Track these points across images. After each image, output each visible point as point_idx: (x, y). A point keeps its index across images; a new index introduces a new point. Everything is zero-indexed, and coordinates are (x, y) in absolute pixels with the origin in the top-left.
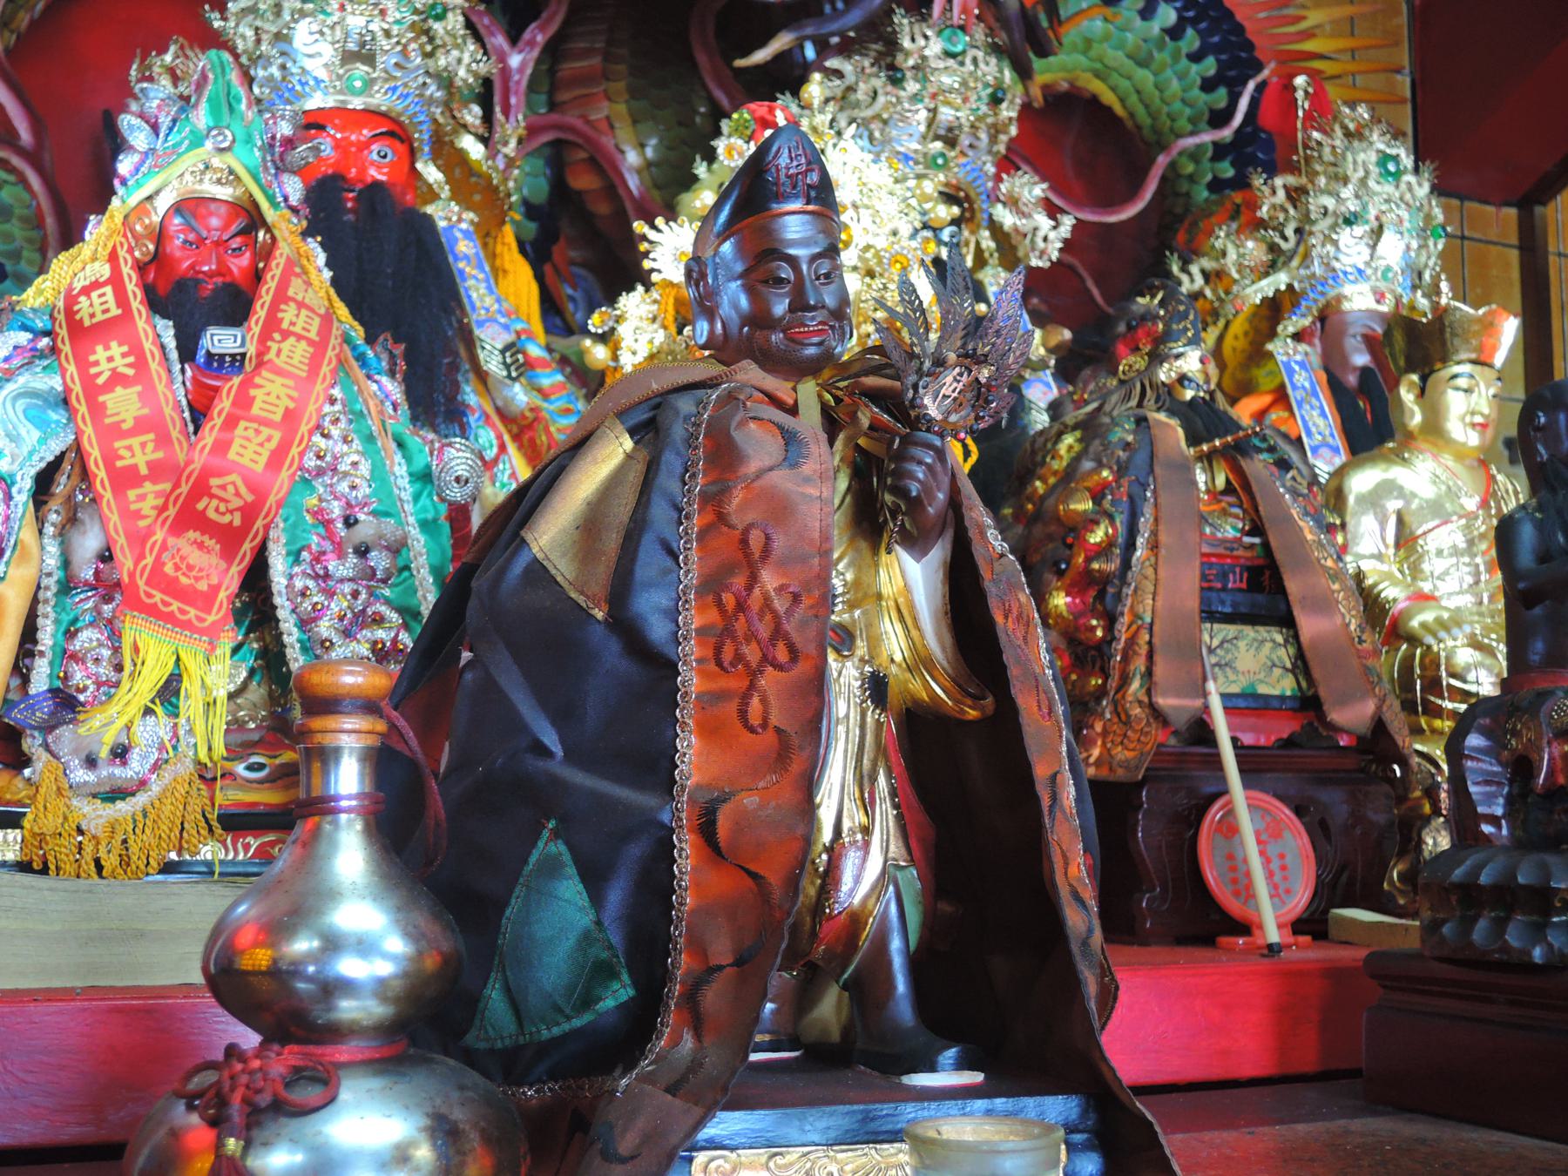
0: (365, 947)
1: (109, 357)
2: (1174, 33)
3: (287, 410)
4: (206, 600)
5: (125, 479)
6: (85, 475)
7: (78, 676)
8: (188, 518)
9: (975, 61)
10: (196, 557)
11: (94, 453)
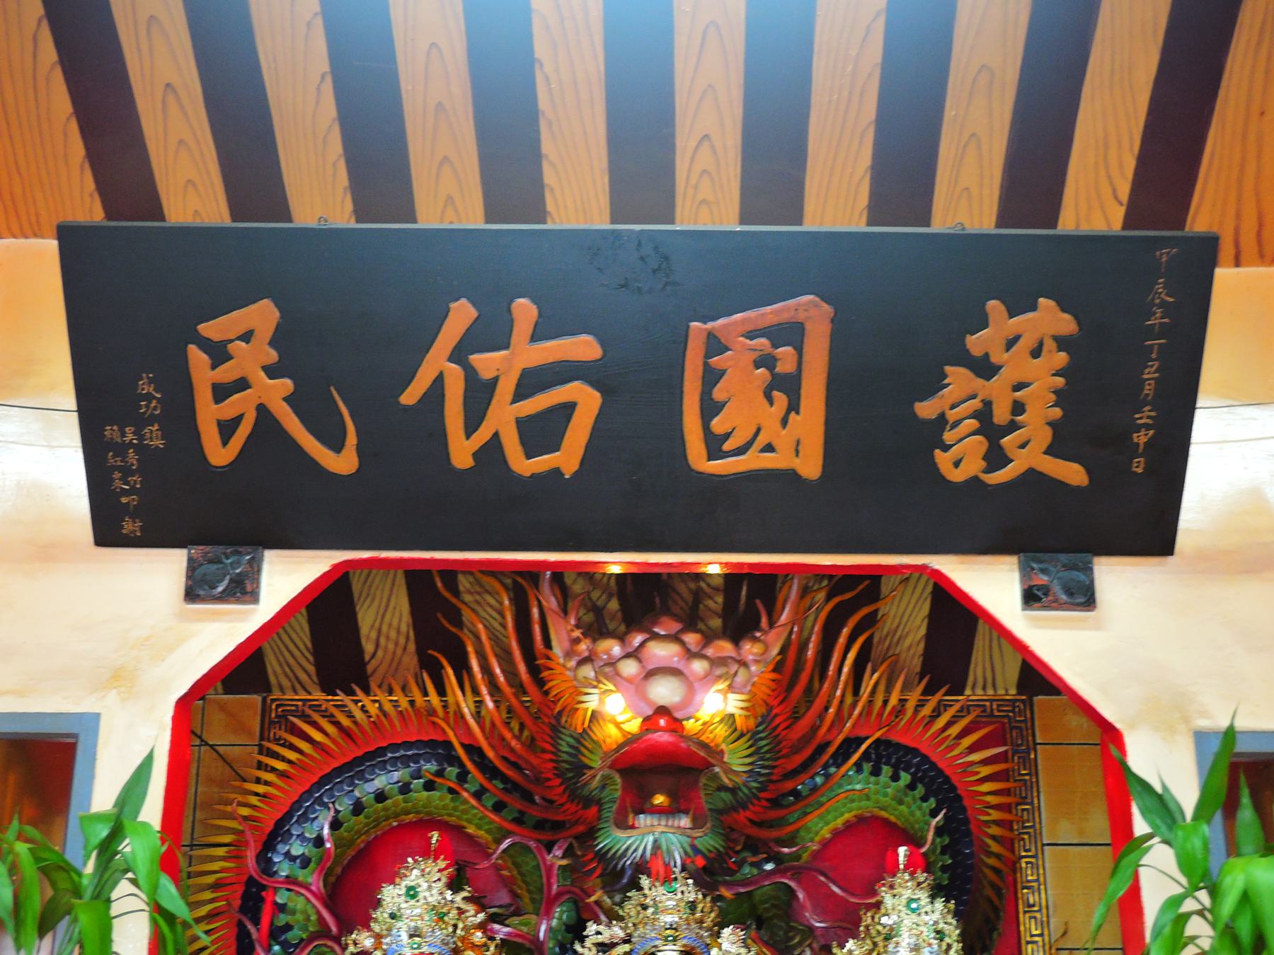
2: (911, 786)
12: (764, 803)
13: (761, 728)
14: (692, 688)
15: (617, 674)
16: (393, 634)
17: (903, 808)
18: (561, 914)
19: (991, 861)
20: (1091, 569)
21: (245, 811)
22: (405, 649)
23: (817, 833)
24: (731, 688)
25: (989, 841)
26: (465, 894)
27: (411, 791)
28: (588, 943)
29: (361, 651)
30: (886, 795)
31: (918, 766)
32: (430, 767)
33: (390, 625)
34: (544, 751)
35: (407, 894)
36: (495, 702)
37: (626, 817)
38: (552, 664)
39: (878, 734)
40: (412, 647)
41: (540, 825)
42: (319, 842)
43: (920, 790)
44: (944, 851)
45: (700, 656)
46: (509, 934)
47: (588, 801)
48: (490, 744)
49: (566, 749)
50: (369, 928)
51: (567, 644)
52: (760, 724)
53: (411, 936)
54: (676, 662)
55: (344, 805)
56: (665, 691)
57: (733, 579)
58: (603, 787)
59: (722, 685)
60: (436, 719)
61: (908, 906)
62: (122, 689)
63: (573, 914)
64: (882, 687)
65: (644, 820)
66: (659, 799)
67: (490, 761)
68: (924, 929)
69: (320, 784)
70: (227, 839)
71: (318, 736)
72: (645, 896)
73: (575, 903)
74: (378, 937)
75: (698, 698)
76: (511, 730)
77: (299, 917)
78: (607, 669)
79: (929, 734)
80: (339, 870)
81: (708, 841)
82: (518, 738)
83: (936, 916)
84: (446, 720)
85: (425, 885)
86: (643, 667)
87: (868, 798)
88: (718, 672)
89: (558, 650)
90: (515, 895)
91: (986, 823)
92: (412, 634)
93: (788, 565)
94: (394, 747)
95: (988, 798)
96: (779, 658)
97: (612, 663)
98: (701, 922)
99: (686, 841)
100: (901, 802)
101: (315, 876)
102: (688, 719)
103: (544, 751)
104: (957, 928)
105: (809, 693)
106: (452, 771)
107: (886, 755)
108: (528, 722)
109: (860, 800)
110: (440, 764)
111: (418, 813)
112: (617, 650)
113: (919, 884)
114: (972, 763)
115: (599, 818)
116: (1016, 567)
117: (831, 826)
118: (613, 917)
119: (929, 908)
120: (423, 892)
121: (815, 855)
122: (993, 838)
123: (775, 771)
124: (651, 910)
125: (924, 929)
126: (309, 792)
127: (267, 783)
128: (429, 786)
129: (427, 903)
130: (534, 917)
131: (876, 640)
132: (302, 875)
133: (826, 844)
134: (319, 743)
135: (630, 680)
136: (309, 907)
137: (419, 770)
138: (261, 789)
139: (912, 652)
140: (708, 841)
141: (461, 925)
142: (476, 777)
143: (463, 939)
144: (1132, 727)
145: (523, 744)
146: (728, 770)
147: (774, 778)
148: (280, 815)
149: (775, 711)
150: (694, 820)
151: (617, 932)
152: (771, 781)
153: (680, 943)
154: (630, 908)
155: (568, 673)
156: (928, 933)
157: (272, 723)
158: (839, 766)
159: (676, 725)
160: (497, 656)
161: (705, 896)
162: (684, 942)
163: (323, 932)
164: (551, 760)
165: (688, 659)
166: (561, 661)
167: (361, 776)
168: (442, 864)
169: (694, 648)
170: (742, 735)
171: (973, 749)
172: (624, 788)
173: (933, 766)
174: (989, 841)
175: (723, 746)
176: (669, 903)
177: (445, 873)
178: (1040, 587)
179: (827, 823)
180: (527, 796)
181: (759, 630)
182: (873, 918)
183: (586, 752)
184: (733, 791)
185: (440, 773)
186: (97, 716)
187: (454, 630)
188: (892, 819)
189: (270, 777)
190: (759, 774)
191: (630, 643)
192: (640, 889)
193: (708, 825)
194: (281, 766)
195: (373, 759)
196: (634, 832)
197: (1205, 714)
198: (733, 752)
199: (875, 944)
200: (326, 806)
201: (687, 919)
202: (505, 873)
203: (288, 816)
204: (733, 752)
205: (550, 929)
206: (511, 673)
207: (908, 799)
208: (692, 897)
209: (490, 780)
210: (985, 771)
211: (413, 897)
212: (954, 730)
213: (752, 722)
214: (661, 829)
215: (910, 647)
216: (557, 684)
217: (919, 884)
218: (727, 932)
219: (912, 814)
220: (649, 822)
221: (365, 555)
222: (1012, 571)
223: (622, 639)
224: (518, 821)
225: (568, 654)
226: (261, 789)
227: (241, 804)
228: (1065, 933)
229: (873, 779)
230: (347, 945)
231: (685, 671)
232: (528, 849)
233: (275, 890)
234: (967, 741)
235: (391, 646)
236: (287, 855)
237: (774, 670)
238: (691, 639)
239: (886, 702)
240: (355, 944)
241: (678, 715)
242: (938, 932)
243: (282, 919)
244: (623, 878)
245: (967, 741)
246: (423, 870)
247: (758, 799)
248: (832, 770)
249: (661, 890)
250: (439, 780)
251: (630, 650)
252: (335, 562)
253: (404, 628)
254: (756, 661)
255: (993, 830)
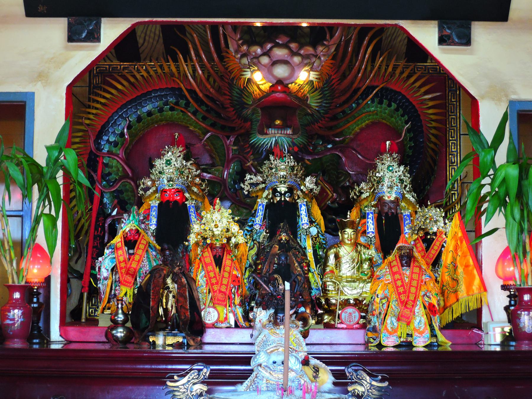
0: (121, 318)
1: (120, 252)
2: (397, 110)
3: (244, 182)
4: (130, 283)
5: (121, 268)
6: (117, 268)
7: (116, 292)
8: (127, 273)
9: (288, 162)
10: (129, 278)
11: (118, 265)
12: (326, 119)
13: (325, 86)
14: (293, 69)
15: (259, 62)
16: (152, 35)
17: (393, 119)
18: (233, 167)
19: (432, 145)
20: (470, 28)
21: (87, 122)
22: (158, 41)
23: (353, 130)
24: (312, 69)
25: (431, 136)
26: (192, 162)
27: (163, 111)
28: (246, 183)
29: (137, 42)
30: (385, 113)
31: (400, 100)
32: (172, 100)
33: (151, 31)
34: (225, 94)
35: (166, 163)
36: (202, 71)
37: (263, 129)
38: (229, 56)
39: (382, 86)
40: (161, 40)
41: (223, 128)
42: (122, 135)
43: (401, 111)
44: (410, 140)
45: (297, 54)
46: (210, 177)
47: (246, 119)
48: (201, 91)
49: (235, 94)
50: (149, 177)
51: (236, 46)
52: (325, 84)
53: (168, 181)
54: (287, 57)
55: (133, 118)
56: (281, 71)
57: (312, 27)
58: (253, 114)
59: (307, 68)
60: (175, 79)
61: (388, 168)
62: (43, 81)
63: (239, 166)
64: (384, 63)
65: (271, 131)
66: (278, 122)
67: (200, 97)
68: (395, 179)
69: (121, 108)
70: (80, 134)
71: (120, 87)
72: (272, 164)
73: (240, 162)
74: (153, 181)
75: (296, 74)
76: (210, 83)
77: (114, 169)
78: (255, 60)
79: (406, 85)
80: (131, 147)
81: (299, 140)
82: (213, 87)
83: (401, 173)
84: (179, 78)
85: (174, 159)
86: (271, 60)
87: (377, 114)
88: (306, 62)
89: (232, 49)
90: (212, 157)
91: (431, 128)
92: (161, 35)
93: (335, 24)
94: (156, 91)
95: (432, 117)
96: (334, 53)
97: (257, 57)
98: (296, 175)
99: (290, 140)
100: (392, 117)
101: (121, 150)
102: (292, 83)
103: (225, 94)
104: (409, 178)
105: (350, 67)
106: (183, 102)
107: (386, 95)
108: (218, 79)
109: (374, 115)
110: (177, 99)
111: (166, 121)
112: (259, 51)
113: (394, 159)
114: (425, 100)
115: (251, 128)
116: (437, 26)
117: (360, 126)
118: (258, 172)
119: (397, 169)
120: (173, 162)
121: (352, 140)
122: (433, 135)
123: (332, 105)
124: (274, 170)
125: (395, 179)
126: (117, 112)
127: (96, 108)
128: (172, 109)
129: (175, 167)
130: (221, 167)
131: (384, 38)
132: (114, 150)
133: (357, 135)
134: (120, 90)
135: (265, 66)
136: (118, 165)
137: (167, 101)
138: (94, 111)
139: (401, 43)
140: (299, 140)
141: (190, 176)
142: (194, 105)
143: (191, 182)
144: (483, 98)
145: (215, 90)
146: (309, 107)
147: (331, 108)
148: (103, 123)
149: (332, 77)
150: (293, 131)
151: (260, 178)
152: (330, 109)
153: (287, 184)
154: (265, 168)
155: (236, 60)
156: (396, 180)
157: (94, 76)
158: (363, 100)
159: (286, 89)
160: (203, 50)
161: (298, 164)
162: (289, 183)
163: (125, 176)
164: (229, 99)
165: (292, 56)
166: (234, 54)
167: (140, 104)
168: (181, 149)
169: (295, 50)
170: (316, 90)
171: (426, 93)
172: (262, 115)
173: (408, 100)
174: (431, 136)
175: (308, 95)
176: (282, 167)
177: (183, 153)
178: (446, 36)
179: (358, 125)
180: (218, 115)
181: (326, 40)
182: (373, 173)
183: (245, 97)
184: (312, 115)
185: (177, 104)
186: (33, 94)
187: (182, 36)
188: (388, 123)
189: (98, 106)
190: (325, 107)
191: (265, 48)
192: (269, 160)
193: (300, 133)
194: (103, 101)
195: (145, 97)
196: (267, 136)
197: (515, 93)
198: (312, 97)
199: (373, 185)
200: (125, 119)
201: (290, 174)
202: (208, 147)
203: (108, 122)
204: (312, 97)
205: (229, 173)
206: (210, 58)
207: (395, 115)
208: (293, 164)
209: (199, 106)
210: (431, 104)
211: (169, 164)
212: (418, 84)
213: (321, 84)
214: (278, 135)
215: (400, 41)
216: (231, 65)
217: (394, 159)
218: (308, 179)
219: (397, 122)
220: (273, 132)
221: (147, 19)
222: (435, 27)
223: (261, 46)
224: (213, 125)
225: (237, 52)
226: (94, 111)
227: (86, 118)
228: (466, 176)
229: (379, 106)
230: (140, 185)
231: (291, 62)
232: (219, 137)
233: (103, 158)
234: (423, 90)
235: (151, 40)
236: (108, 141)
237: (332, 59)
238: (293, 45)
239: (386, 70)
240: (143, 184)
241: (286, 82)
242: (401, 180)
243: (107, 170)
244: (262, 156)
245: (423, 90)
246: (173, 152)
247: (324, 118)
248: (360, 101)
249: (279, 161)
250: (176, 107)
251: (265, 51)
252: (133, 23)
253: (157, 32)
254: (324, 55)
255: (433, 131)
